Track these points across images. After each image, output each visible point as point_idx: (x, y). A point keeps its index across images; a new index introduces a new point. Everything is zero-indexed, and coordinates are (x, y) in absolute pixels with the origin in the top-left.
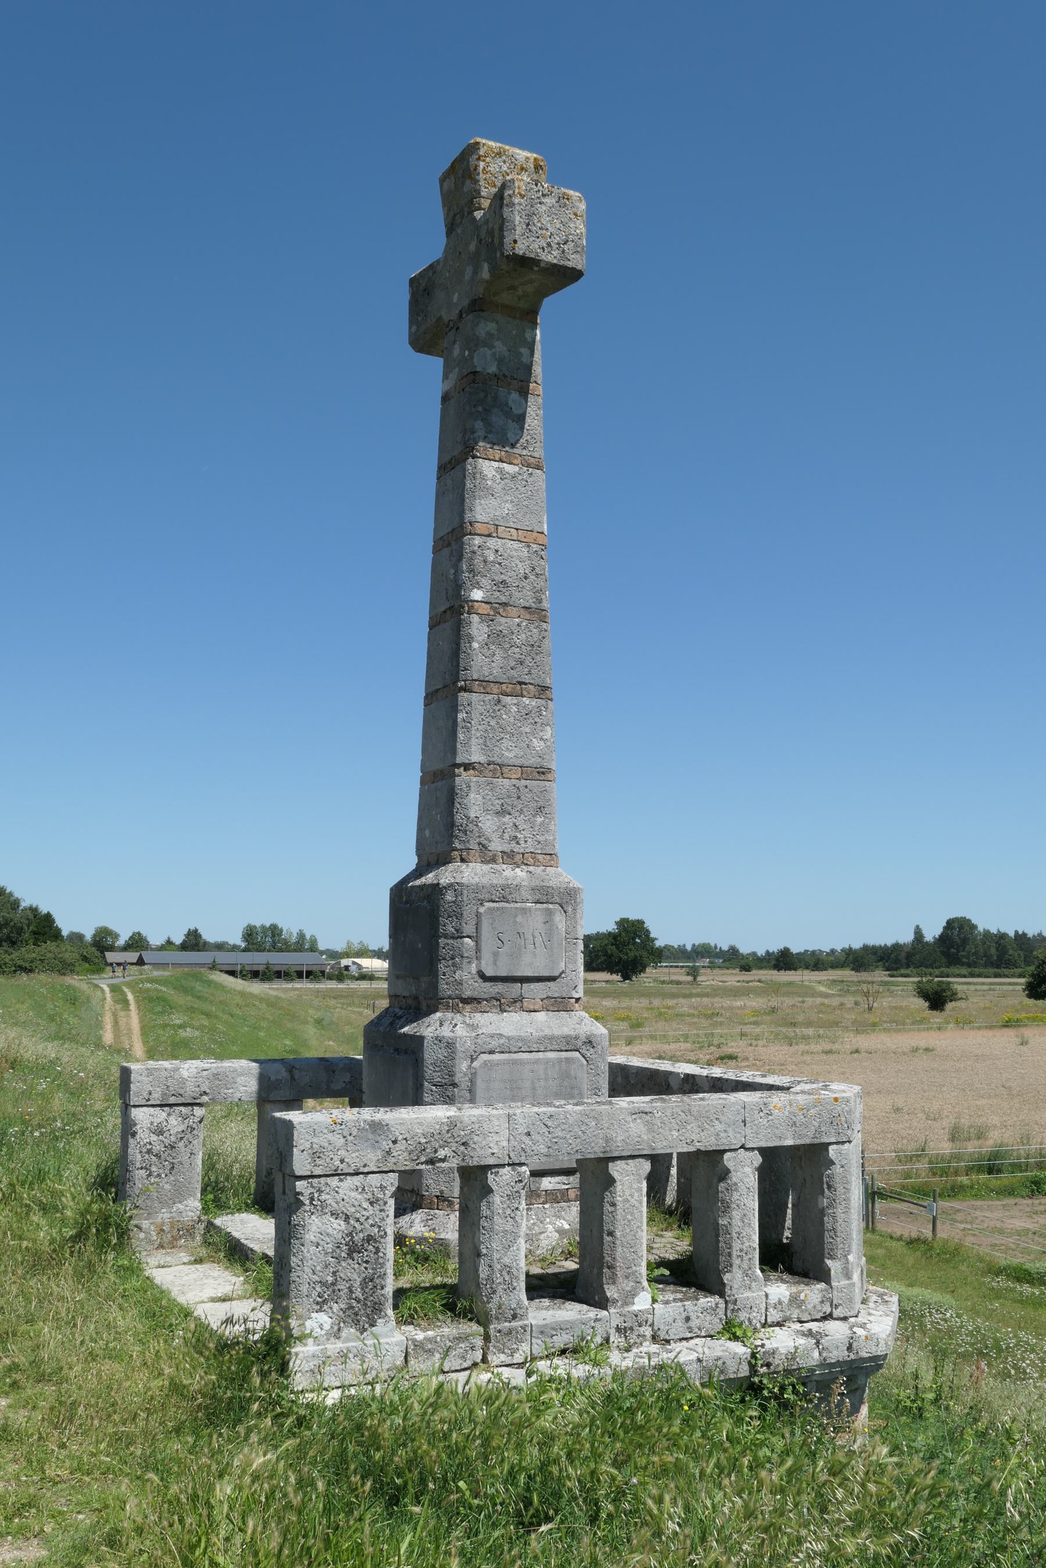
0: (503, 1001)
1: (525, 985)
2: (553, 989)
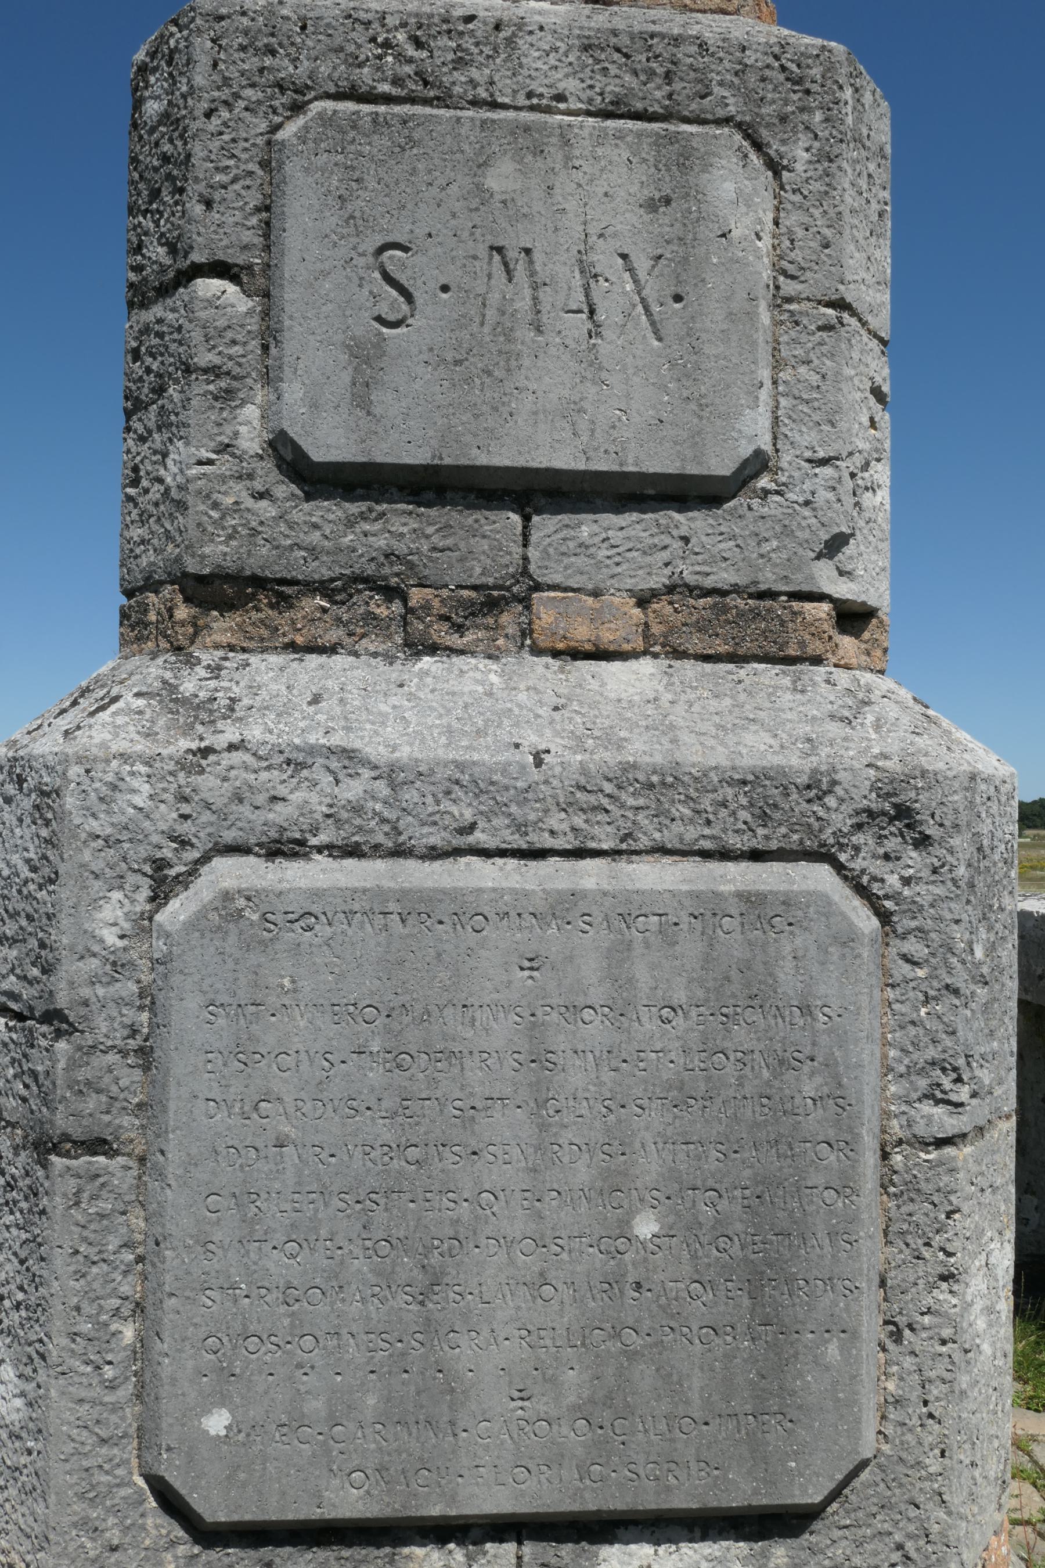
0: (416, 596)
1: (545, 525)
2: (710, 546)
